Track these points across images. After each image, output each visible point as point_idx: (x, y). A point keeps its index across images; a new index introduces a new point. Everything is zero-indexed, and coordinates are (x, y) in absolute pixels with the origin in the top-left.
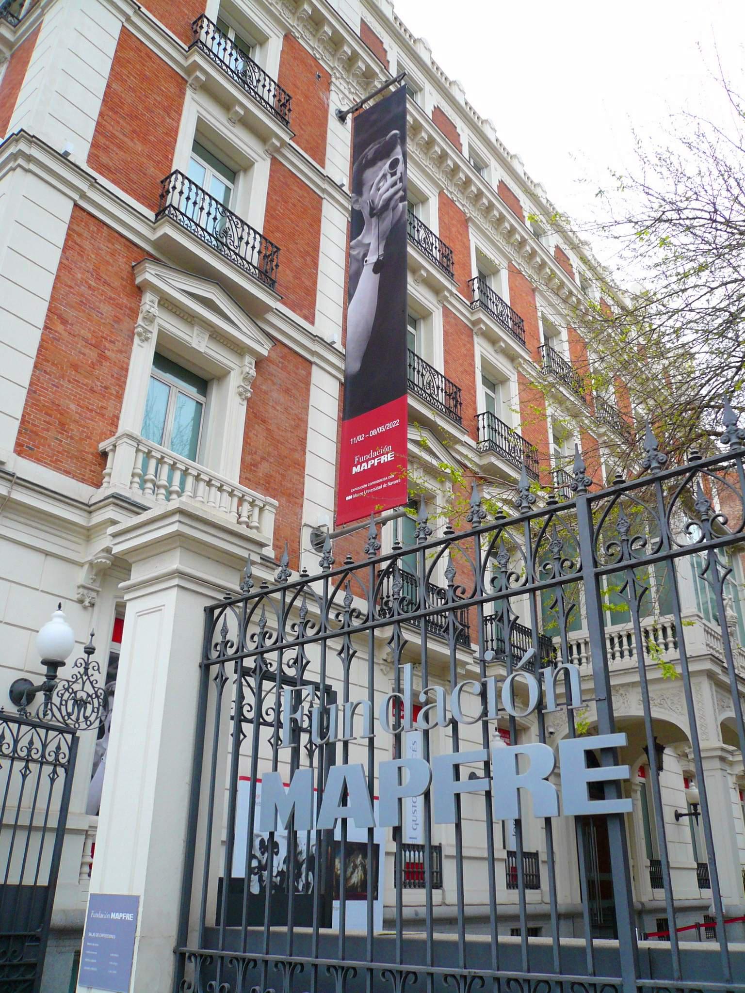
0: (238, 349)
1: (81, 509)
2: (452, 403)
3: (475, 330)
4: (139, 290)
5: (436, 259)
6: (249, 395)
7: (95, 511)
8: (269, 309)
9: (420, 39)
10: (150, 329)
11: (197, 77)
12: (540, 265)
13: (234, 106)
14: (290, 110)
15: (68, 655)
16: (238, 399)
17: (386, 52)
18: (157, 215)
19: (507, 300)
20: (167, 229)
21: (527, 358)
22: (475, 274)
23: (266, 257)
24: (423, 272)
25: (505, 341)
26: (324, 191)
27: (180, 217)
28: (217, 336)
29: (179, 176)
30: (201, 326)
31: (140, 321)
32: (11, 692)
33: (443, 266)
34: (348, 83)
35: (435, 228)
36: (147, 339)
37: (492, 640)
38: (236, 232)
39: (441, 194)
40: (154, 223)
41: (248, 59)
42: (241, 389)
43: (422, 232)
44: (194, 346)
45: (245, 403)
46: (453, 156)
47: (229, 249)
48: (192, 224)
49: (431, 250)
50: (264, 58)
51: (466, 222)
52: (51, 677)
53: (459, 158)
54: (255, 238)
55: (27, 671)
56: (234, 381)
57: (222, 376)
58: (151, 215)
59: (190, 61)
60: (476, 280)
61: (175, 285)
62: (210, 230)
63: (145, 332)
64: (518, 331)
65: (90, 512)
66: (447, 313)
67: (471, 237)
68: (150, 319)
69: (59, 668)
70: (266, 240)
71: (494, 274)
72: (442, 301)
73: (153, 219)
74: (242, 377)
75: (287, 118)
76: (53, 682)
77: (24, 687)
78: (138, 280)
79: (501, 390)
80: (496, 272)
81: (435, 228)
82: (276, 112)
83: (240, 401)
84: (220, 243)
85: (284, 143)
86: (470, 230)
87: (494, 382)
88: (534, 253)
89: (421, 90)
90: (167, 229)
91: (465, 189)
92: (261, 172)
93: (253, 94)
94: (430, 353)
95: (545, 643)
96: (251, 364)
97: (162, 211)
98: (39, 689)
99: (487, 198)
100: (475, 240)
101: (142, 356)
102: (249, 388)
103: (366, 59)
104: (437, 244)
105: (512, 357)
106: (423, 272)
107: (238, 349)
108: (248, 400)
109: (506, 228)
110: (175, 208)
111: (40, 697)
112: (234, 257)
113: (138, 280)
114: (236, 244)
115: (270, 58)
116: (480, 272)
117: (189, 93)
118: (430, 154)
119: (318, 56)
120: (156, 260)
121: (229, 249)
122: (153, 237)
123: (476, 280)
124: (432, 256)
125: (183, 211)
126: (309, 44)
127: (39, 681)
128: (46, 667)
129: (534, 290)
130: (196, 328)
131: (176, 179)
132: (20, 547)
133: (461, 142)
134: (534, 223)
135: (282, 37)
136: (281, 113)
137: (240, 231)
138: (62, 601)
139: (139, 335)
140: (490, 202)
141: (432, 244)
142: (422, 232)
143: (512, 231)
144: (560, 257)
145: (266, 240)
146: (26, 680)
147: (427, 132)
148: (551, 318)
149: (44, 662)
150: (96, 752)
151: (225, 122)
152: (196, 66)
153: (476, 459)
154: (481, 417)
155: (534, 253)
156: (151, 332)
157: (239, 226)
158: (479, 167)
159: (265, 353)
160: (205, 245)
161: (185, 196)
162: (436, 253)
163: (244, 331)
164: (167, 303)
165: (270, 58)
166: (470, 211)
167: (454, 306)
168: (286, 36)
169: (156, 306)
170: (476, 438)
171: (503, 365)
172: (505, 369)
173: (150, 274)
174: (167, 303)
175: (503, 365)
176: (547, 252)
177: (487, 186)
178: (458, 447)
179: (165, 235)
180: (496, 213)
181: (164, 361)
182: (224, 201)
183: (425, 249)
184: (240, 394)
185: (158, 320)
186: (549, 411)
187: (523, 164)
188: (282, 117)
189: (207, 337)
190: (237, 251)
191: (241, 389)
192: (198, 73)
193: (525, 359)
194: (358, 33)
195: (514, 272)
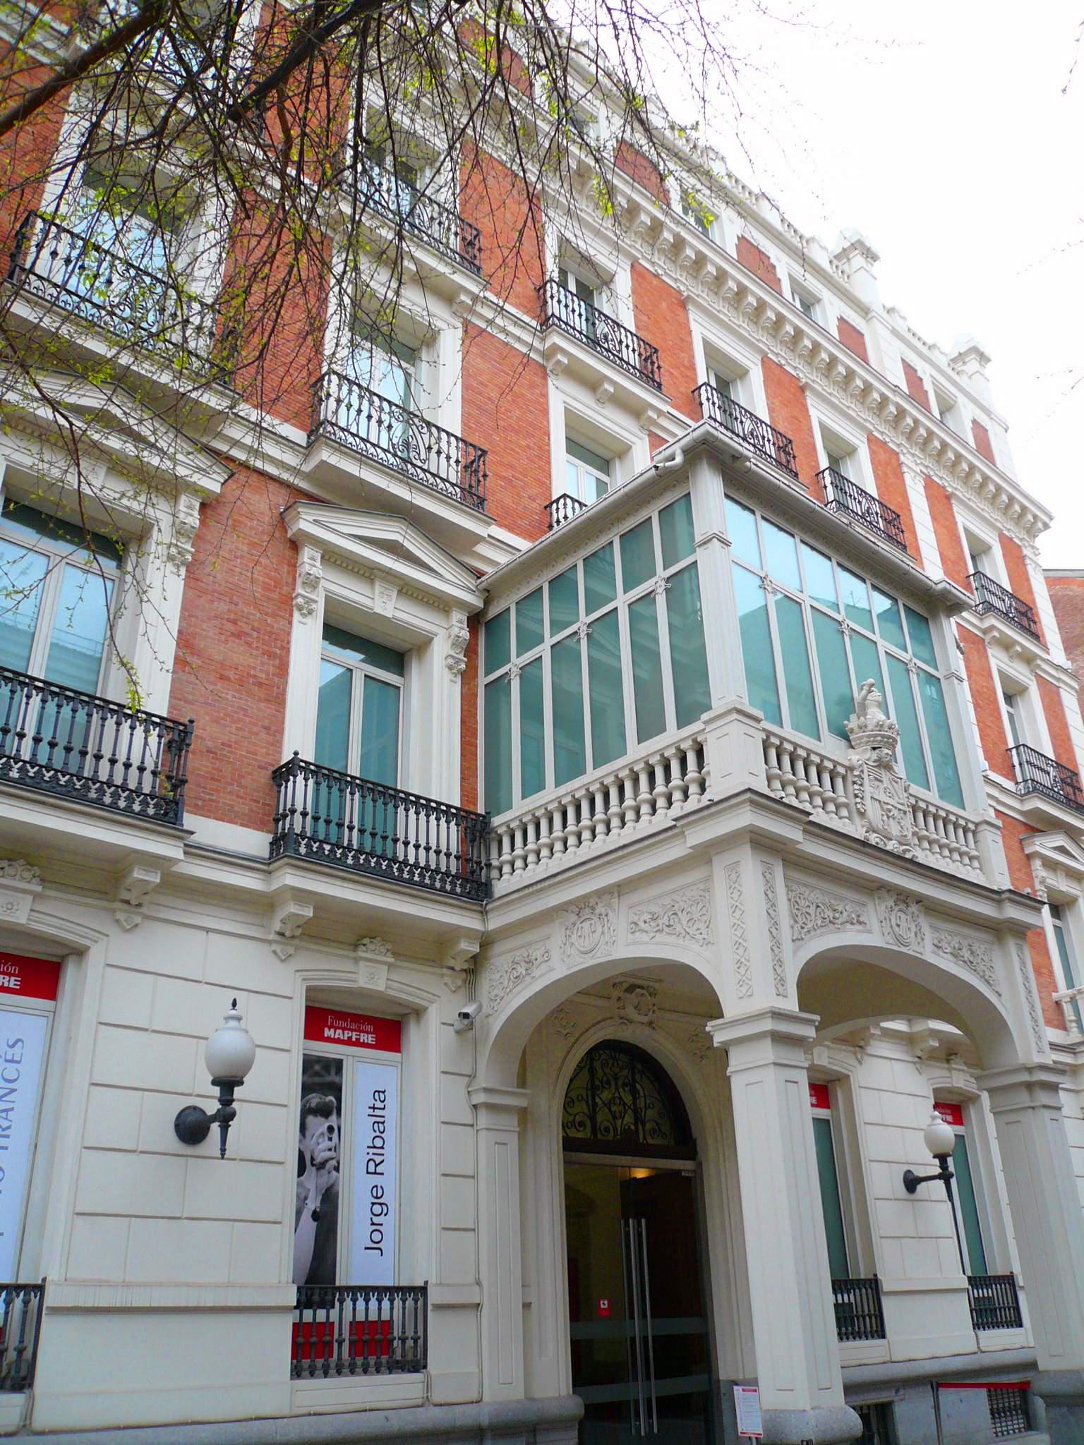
1: (258, 870)
2: (1069, 789)
4: (295, 545)
5: (770, 456)
6: (189, 557)
7: (276, 870)
8: (479, 539)
9: (813, 238)
10: (314, 597)
11: (559, 362)
13: (646, 411)
14: (480, 250)
16: (448, 675)
17: (774, 267)
19: (873, 490)
20: (326, 455)
21: (665, 408)
22: (824, 463)
23: (469, 468)
24: (607, 386)
26: (1059, 679)
28: (409, 590)
29: (569, 501)
30: (383, 579)
31: (300, 590)
32: (177, 1126)
34: (913, 455)
36: (310, 612)
37: (351, 828)
41: (590, 307)
42: (450, 661)
43: (747, 423)
44: (378, 610)
47: (414, 465)
49: (620, 351)
50: (859, 471)
52: (226, 1100)
54: (449, 442)
55: (198, 1096)
56: (162, 536)
57: (422, 645)
58: (299, 436)
60: (827, 473)
61: (342, 530)
62: (384, 444)
65: (270, 873)
66: (472, 335)
67: (694, 326)
68: (313, 583)
69: (236, 1089)
71: (984, 552)
75: (477, 262)
77: (191, 1118)
79: (1020, 702)
80: (852, 451)
82: (462, 257)
83: (452, 677)
85: (475, 298)
86: (691, 316)
88: (701, 260)
89: (819, 300)
90: (326, 455)
91: (677, 255)
92: (450, 343)
93: (426, 238)
95: (476, 829)
96: (460, 622)
97: (316, 430)
98: (213, 1118)
99: (692, 247)
101: (306, 637)
102: (461, 656)
103: (757, 290)
105: (635, 410)
106: (607, 386)
107: (171, 488)
108: (190, 567)
110: (332, 424)
111: (215, 1128)
112: (422, 475)
114: (423, 456)
115: (620, 304)
116: (830, 456)
117: (551, 382)
118: (679, 262)
119: (660, 272)
121: (414, 465)
122: (306, 468)
123: (827, 473)
124: (621, 359)
125: (434, 470)
126: (659, 265)
127: (212, 1107)
129: (802, 389)
130: (377, 584)
131: (565, 504)
133: (779, 275)
134: (795, 285)
137: (426, 437)
139: (300, 609)
140: (739, 284)
141: (763, 437)
142: (747, 423)
144: (751, 256)
146: (195, 1108)
148: (976, 531)
151: (594, 405)
152: (556, 348)
155: (868, 388)
156: (316, 602)
157: (425, 430)
158: (808, 304)
159: (216, 488)
160: (381, 467)
164: (334, 558)
165: (620, 304)
166: (803, 373)
168: (632, 266)
169: (318, 564)
170: (1012, 777)
171: (1020, 672)
172: (608, 424)
173: (307, 521)
174: (334, 558)
175: (1020, 672)
177: (823, 331)
178: (481, 549)
179: (323, 463)
180: (751, 299)
181: (335, 633)
183: (754, 446)
184: (450, 668)
186: (994, 664)
187: (904, 318)
190: (425, 467)
191: (450, 661)
192: (559, 357)
193: (660, 413)
194: (905, 388)
195: (773, 372)
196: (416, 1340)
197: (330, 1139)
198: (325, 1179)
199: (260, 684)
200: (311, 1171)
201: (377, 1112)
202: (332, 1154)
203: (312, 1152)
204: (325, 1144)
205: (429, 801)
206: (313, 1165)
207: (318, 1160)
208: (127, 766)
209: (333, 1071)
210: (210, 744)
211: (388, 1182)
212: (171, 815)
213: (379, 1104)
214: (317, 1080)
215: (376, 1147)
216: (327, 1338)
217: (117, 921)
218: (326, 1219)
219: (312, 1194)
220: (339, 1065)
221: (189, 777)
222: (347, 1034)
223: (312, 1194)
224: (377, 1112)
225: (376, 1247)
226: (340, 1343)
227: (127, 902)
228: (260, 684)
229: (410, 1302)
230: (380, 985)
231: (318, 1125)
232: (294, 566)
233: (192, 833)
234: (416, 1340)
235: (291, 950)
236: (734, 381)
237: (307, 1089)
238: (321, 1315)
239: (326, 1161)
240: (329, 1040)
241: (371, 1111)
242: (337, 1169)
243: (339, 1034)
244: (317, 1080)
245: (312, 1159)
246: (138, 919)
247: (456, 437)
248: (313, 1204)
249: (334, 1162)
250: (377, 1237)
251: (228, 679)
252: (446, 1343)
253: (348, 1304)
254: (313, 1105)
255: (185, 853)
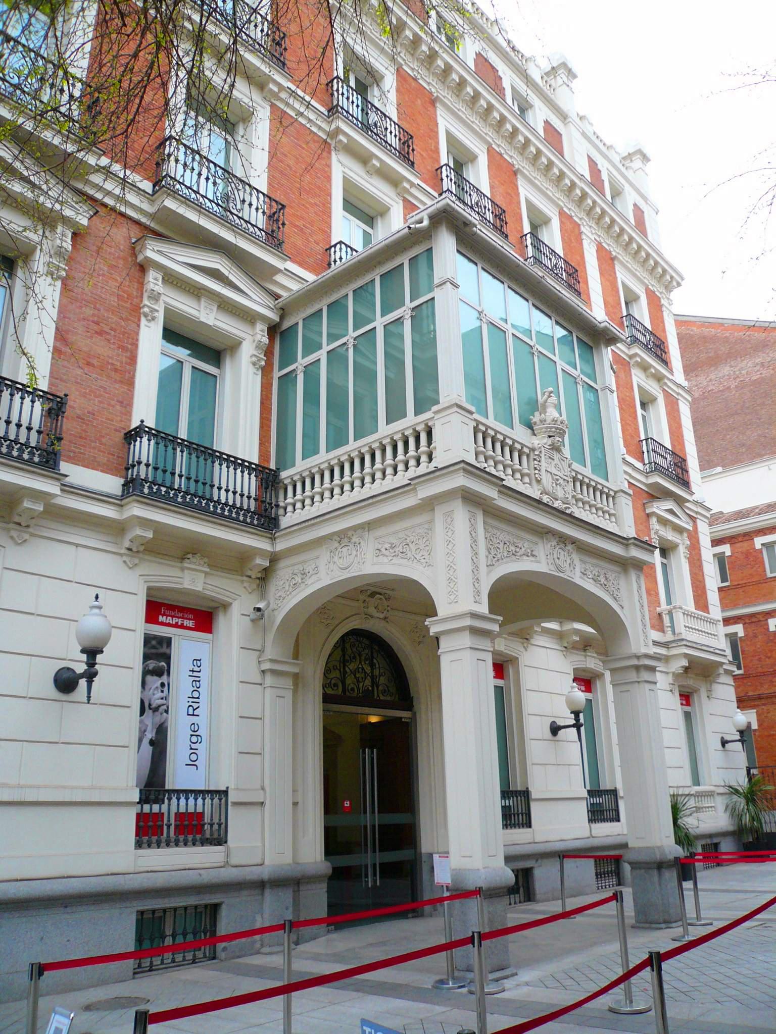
0: (47, 220)
2: (680, 471)
3: (632, 362)
4: (142, 268)
5: (489, 222)
6: (64, 274)
10: (156, 307)
11: (341, 141)
12: (473, 97)
13: (401, 182)
15: (106, 644)
16: (252, 369)
17: (501, 78)
18: (154, 186)
21: (417, 181)
22: (527, 229)
25: (654, 367)
26: (678, 394)
27: (178, 186)
28: (226, 306)
31: (146, 302)
33: (497, 228)
34: (590, 227)
35: (392, 112)
36: (153, 319)
38: (239, 196)
39: (562, 213)
40: (152, 195)
42: (254, 359)
43: (474, 196)
44: (202, 319)
45: (260, 372)
46: (445, 55)
47: (232, 213)
48: (206, 201)
49: (385, 136)
51: (433, 102)
52: (91, 664)
53: (506, 108)
57: (234, 346)
58: (147, 186)
59: (333, 126)
60: (529, 236)
63: (151, 311)
64: (572, 282)
68: (155, 297)
70: (270, 198)
72: (271, 98)
73: (150, 192)
74: (254, 345)
76: (92, 670)
77: (66, 675)
78: (140, 258)
80: (547, 221)
81: (392, 112)
83: (255, 370)
84: (225, 212)
86: (439, 112)
87: (372, 213)
88: (448, 69)
94: (660, 432)
98: (82, 676)
100: (444, 123)
102: (262, 356)
104: (489, 205)
105: (394, 181)
109: (507, 130)
111: (83, 682)
113: (140, 258)
114: (239, 207)
120: (158, 235)
123: (529, 236)
124: (386, 142)
127: (80, 668)
128: (85, 656)
129: (515, 173)
130: (203, 300)
132: (104, 554)
135: (486, 151)
136: (405, 156)
137: (241, 193)
138: (98, 591)
139: (146, 315)
141: (485, 207)
142: (474, 196)
143: (416, 41)
145: (270, 198)
146: (68, 669)
147: (457, 73)
149: (83, 651)
150: (140, 728)
153: (643, 479)
154: (333, 249)
155: (490, 108)
156: (157, 311)
157: (240, 187)
159: (85, 222)
160: (208, 214)
161: (254, 207)
162: (489, 216)
163: (52, 195)
164: (172, 279)
166: (517, 161)
167: (416, 198)
169: (160, 283)
171: (653, 387)
173: (152, 251)
174: (172, 279)
175: (653, 387)
176: (533, 130)
178: (279, 278)
182: (225, 164)
184: (254, 364)
185: (163, 297)
188: (278, 59)
189: (215, 308)
190: (240, 215)
191: (254, 359)
193: (412, 185)
196: (220, 825)
197: (162, 692)
198: (158, 719)
199: (116, 370)
200: (148, 712)
201: (195, 674)
202: (164, 701)
203: (150, 700)
204: (160, 695)
205: (243, 461)
206: (150, 709)
207: (154, 706)
208: (19, 426)
209: (165, 645)
210: (78, 412)
211: (202, 720)
212: (51, 462)
213: (196, 669)
214: (154, 651)
215: (195, 698)
216: (160, 823)
217: (12, 538)
218: (159, 745)
219: (149, 728)
220: (168, 641)
221: (64, 435)
222: (175, 620)
223: (149, 728)
224: (195, 674)
225: (193, 764)
226: (169, 826)
227: (19, 524)
228: (116, 370)
229: (216, 800)
230: (199, 587)
231: (154, 682)
232: (141, 284)
233: (66, 476)
234: (220, 825)
235: (137, 561)
236: (466, 163)
237: (146, 657)
238: (156, 808)
239: (159, 706)
240: (162, 624)
241: (191, 673)
242: (167, 711)
243: (169, 620)
244: (154, 651)
245: (150, 705)
246: (27, 536)
247: (264, 194)
248: (150, 735)
249: (165, 707)
250: (194, 757)
251: (93, 366)
252: (239, 826)
253: (174, 800)
254: (151, 668)
255: (61, 490)
